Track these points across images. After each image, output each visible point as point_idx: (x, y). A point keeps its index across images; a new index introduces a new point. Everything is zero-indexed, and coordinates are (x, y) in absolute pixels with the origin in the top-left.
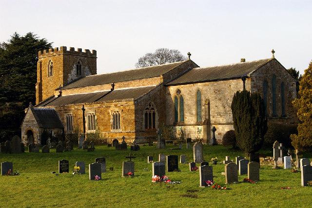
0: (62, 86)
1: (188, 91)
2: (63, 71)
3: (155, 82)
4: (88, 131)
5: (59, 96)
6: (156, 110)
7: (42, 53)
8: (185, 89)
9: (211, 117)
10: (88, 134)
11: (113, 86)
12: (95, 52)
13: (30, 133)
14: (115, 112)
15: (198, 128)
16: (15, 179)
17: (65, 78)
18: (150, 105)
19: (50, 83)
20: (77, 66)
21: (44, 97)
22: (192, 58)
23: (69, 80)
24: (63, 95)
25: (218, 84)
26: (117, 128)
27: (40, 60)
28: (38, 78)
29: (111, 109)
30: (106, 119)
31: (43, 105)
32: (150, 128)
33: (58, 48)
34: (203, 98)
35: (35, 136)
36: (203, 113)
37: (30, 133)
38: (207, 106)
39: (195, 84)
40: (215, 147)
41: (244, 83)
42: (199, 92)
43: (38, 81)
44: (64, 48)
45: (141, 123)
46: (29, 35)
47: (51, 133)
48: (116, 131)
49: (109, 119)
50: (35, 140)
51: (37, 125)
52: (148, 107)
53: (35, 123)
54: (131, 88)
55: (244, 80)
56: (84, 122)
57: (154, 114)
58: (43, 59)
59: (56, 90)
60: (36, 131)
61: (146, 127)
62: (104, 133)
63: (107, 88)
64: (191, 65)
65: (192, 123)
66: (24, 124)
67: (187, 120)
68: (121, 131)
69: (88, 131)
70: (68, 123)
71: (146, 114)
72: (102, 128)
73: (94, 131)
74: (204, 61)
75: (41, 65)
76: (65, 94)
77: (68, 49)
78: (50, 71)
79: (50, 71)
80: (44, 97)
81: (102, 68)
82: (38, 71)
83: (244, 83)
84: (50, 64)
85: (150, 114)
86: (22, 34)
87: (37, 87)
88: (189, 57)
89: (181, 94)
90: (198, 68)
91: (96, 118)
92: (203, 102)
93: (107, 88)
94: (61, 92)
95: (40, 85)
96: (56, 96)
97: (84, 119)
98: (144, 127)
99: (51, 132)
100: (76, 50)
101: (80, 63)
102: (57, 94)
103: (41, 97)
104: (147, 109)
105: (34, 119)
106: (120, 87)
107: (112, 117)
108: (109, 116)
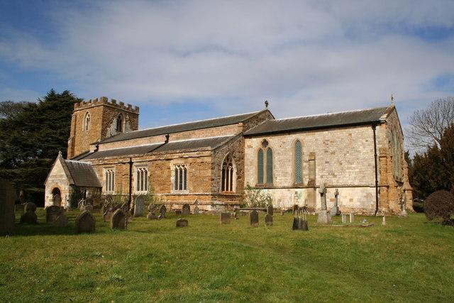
3: (231, 132)
4: (135, 192)
5: (96, 151)
9: (317, 177)
10: (135, 196)
11: (168, 137)
12: (137, 109)
13: (56, 192)
14: (179, 166)
15: (296, 193)
16: (84, 125)
17: (104, 132)
19: (84, 128)
22: (269, 108)
23: (108, 135)
26: (142, 189)
28: (72, 132)
30: (165, 175)
32: (227, 190)
33: (97, 100)
34: (305, 150)
35: (63, 196)
36: (305, 172)
37: (56, 192)
43: (72, 136)
44: (105, 100)
46: (66, 93)
47: (85, 193)
48: (178, 192)
49: (169, 176)
50: (63, 201)
53: (65, 178)
54: (193, 139)
56: (131, 180)
57: (232, 171)
58: (78, 113)
61: (223, 190)
62: (159, 195)
63: (159, 140)
64: (267, 114)
65: (286, 185)
66: (50, 179)
67: (277, 180)
68: (186, 192)
69: (135, 192)
70: (107, 181)
72: (157, 188)
73: (145, 192)
76: (102, 148)
80: (77, 153)
82: (73, 124)
84: (87, 117)
86: (59, 92)
87: (69, 142)
91: (148, 175)
92: (306, 158)
93: (159, 140)
94: (97, 147)
95: (73, 139)
96: (92, 151)
97: (131, 175)
99: (86, 191)
101: (120, 116)
102: (92, 149)
103: (73, 153)
105: (64, 173)
106: (178, 138)
107: (173, 173)
108: (170, 172)
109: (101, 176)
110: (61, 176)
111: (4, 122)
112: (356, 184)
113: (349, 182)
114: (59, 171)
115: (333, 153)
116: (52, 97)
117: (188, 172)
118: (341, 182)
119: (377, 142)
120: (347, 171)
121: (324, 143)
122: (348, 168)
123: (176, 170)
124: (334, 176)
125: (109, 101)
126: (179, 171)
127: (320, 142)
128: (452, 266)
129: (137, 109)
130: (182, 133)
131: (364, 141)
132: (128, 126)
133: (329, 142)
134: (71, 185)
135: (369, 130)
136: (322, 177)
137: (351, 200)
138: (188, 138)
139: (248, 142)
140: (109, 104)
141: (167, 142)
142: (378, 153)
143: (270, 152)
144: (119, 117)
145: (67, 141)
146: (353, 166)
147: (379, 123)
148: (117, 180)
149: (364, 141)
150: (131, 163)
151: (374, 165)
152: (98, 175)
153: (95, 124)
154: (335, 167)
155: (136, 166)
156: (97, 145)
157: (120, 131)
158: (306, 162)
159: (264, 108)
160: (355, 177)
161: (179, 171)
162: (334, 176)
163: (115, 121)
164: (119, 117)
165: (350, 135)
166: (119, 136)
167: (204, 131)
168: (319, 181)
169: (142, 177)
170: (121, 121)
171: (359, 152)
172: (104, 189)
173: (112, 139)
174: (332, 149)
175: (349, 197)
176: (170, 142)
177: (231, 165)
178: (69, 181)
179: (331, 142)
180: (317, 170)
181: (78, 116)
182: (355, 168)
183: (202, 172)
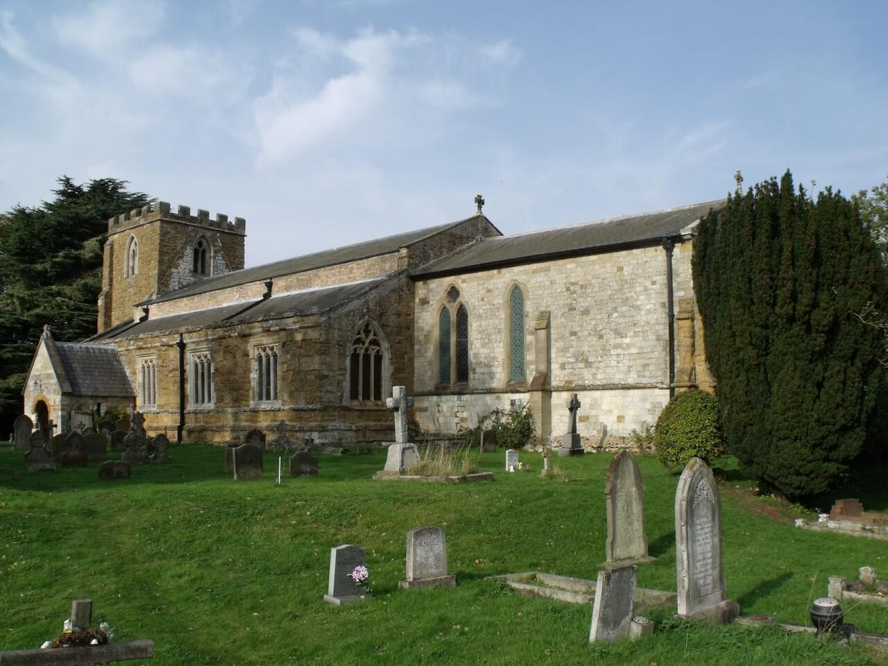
0: (154, 297)
1: (483, 294)
2: (159, 262)
5: (143, 319)
6: (385, 345)
7: (117, 222)
8: (471, 288)
9: (554, 367)
11: (269, 286)
12: (241, 223)
13: (41, 408)
14: (264, 350)
18: (367, 332)
20: (196, 251)
21: (115, 323)
22: (487, 212)
23: (174, 284)
24: (152, 317)
25: (57, 417)
27: (110, 239)
29: (253, 341)
31: (109, 335)
34: (529, 307)
36: (530, 356)
38: (542, 333)
39: (504, 271)
40: (575, 459)
41: (670, 256)
42: (516, 297)
45: (339, 382)
49: (247, 371)
51: (57, 388)
52: (363, 335)
53: (54, 380)
55: (669, 250)
56: (183, 381)
57: (379, 358)
59: (137, 306)
60: (54, 400)
61: (354, 396)
64: (479, 227)
67: (477, 376)
71: (355, 357)
74: (514, 221)
75: (112, 248)
76: (156, 313)
77: (175, 210)
78: (131, 264)
79: (131, 264)
80: (115, 323)
81: (256, 253)
83: (670, 256)
85: (367, 357)
87: (100, 302)
88: (480, 207)
89: (460, 299)
90: (501, 237)
92: (530, 323)
94: (146, 311)
95: (109, 296)
97: (183, 371)
98: (347, 394)
100: (194, 213)
102: (138, 315)
104: (358, 341)
105: (52, 371)
106: (287, 288)
108: (248, 362)
109: (134, 373)
110: (48, 376)
111: (3, 260)
112: (631, 381)
113: (618, 378)
114: (44, 367)
115: (586, 312)
116: (71, 193)
117: (279, 361)
118: (601, 378)
119: (674, 285)
120: (613, 352)
121: (568, 289)
122: (616, 347)
123: (260, 359)
124: (588, 364)
125: (175, 210)
126: (264, 359)
127: (560, 287)
128: (405, 663)
129: (241, 223)
130: (294, 276)
131: (648, 284)
132: (221, 262)
133: (577, 288)
134: (64, 394)
135: (658, 253)
136: (563, 367)
137: (620, 419)
138: (307, 286)
139: (421, 289)
140: (173, 216)
141: (267, 296)
142: (676, 309)
143: (462, 315)
144: (200, 244)
145: (96, 302)
146: (627, 340)
147: (679, 239)
148: (161, 381)
149: (648, 284)
150: (182, 346)
151: (667, 337)
152: (128, 372)
153: (146, 261)
154: (588, 345)
155: (194, 351)
156: (145, 306)
157: (203, 272)
158: (531, 333)
159: (473, 211)
160: (630, 367)
161: (264, 359)
162: (588, 364)
163: (189, 252)
164: (200, 244)
165: (620, 269)
166: (200, 280)
167: (336, 269)
168: (558, 377)
169: (203, 374)
170: (204, 252)
171: (638, 308)
172: (139, 401)
173: (188, 290)
174: (582, 304)
175: (616, 413)
176: (274, 296)
177: (375, 342)
178: (61, 387)
179: (582, 287)
180: (553, 351)
181: (116, 247)
182: (629, 346)
183: (303, 360)
